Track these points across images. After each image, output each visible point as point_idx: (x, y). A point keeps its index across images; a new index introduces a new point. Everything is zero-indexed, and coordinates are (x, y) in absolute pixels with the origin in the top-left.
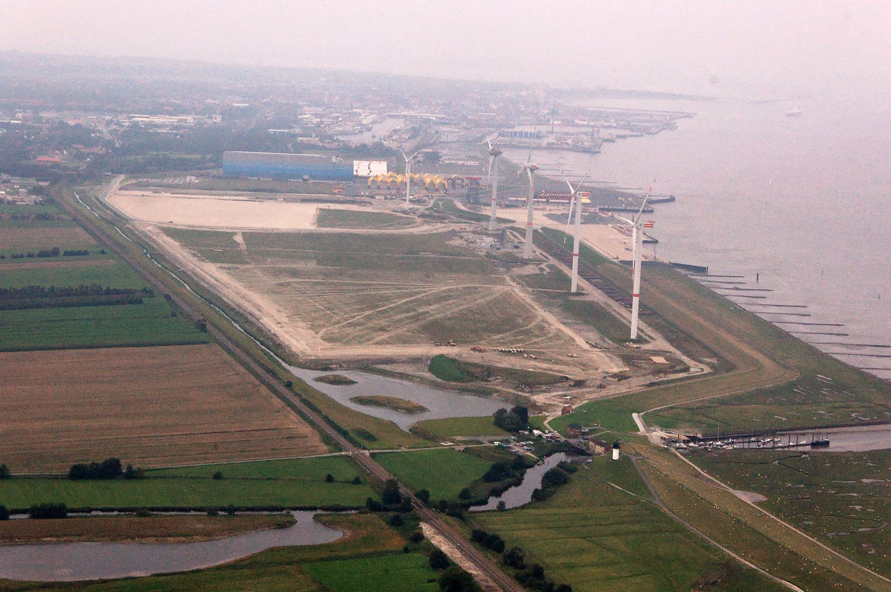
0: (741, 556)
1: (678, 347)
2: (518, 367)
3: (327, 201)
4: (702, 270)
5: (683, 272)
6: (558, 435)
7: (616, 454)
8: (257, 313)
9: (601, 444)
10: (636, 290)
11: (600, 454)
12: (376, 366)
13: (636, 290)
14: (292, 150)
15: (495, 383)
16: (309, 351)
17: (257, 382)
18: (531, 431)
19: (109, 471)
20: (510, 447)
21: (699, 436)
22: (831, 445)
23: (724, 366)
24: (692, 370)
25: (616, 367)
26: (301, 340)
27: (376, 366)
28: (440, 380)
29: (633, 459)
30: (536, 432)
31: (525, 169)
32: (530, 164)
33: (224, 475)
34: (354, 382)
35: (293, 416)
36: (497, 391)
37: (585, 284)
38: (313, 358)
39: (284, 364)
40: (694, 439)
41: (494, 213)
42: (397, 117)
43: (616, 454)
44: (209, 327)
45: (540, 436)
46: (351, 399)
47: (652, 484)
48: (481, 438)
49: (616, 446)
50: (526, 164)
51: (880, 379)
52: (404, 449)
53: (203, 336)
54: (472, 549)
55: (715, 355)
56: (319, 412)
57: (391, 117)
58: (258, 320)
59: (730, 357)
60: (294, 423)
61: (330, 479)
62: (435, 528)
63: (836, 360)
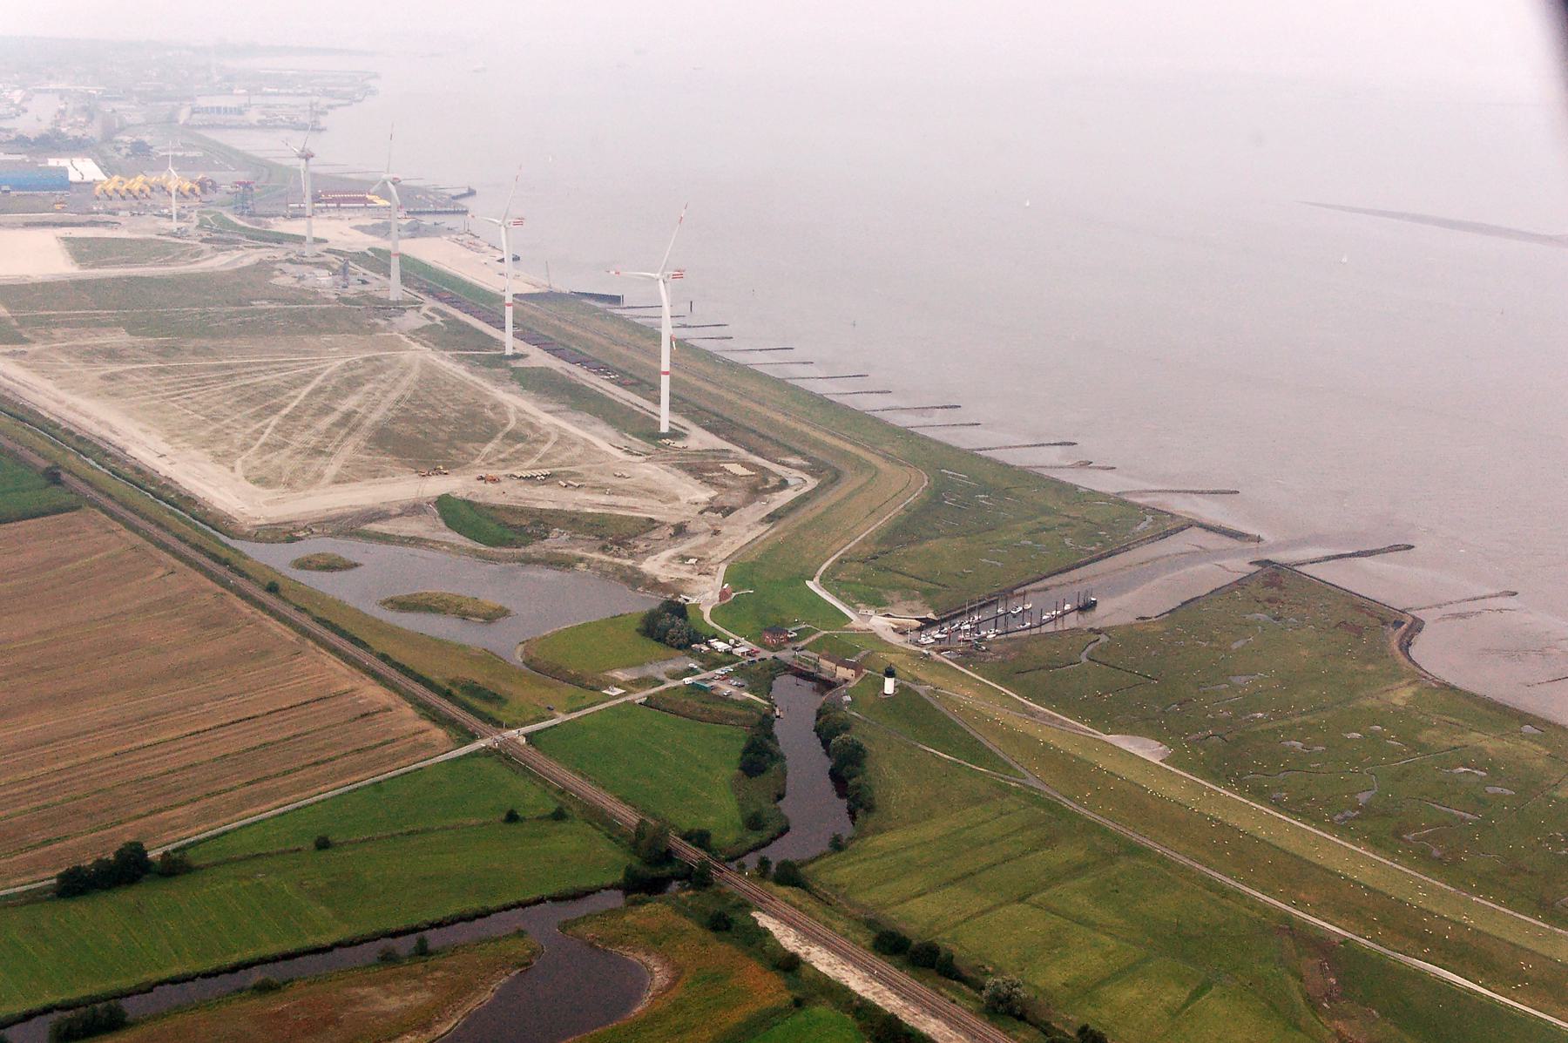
0: (1294, 906)
1: (730, 440)
2: (570, 507)
3: (72, 225)
4: (616, 300)
5: (599, 305)
6: (755, 648)
7: (889, 686)
8: (106, 433)
9: (848, 666)
10: (665, 365)
11: (846, 681)
12: (367, 527)
13: (665, 365)
14: (395, 261)
15: (558, 542)
16: (247, 509)
17: (219, 589)
18: (708, 644)
19: (129, 869)
20: (713, 688)
21: (931, 615)
22: (1100, 610)
23: (827, 472)
24: (791, 482)
25: (704, 495)
26: (225, 489)
27: (367, 527)
28: (482, 548)
29: (921, 690)
30: (721, 646)
31: (385, 183)
32: (391, 176)
33: (334, 838)
34: (356, 565)
35: (332, 661)
36: (581, 560)
37: (523, 347)
38: (263, 522)
39: (223, 538)
40: (928, 624)
41: (310, 229)
42: (47, 91)
43: (889, 686)
44: (65, 476)
45: (728, 653)
46: (384, 603)
47: (992, 743)
48: (651, 670)
50: (385, 176)
51: (965, 452)
52: (561, 718)
53: (57, 495)
54: (881, 964)
55: (794, 452)
56: (364, 645)
57: (40, 91)
58: (123, 451)
59: (815, 453)
60: (336, 673)
61: (512, 817)
62: (795, 927)
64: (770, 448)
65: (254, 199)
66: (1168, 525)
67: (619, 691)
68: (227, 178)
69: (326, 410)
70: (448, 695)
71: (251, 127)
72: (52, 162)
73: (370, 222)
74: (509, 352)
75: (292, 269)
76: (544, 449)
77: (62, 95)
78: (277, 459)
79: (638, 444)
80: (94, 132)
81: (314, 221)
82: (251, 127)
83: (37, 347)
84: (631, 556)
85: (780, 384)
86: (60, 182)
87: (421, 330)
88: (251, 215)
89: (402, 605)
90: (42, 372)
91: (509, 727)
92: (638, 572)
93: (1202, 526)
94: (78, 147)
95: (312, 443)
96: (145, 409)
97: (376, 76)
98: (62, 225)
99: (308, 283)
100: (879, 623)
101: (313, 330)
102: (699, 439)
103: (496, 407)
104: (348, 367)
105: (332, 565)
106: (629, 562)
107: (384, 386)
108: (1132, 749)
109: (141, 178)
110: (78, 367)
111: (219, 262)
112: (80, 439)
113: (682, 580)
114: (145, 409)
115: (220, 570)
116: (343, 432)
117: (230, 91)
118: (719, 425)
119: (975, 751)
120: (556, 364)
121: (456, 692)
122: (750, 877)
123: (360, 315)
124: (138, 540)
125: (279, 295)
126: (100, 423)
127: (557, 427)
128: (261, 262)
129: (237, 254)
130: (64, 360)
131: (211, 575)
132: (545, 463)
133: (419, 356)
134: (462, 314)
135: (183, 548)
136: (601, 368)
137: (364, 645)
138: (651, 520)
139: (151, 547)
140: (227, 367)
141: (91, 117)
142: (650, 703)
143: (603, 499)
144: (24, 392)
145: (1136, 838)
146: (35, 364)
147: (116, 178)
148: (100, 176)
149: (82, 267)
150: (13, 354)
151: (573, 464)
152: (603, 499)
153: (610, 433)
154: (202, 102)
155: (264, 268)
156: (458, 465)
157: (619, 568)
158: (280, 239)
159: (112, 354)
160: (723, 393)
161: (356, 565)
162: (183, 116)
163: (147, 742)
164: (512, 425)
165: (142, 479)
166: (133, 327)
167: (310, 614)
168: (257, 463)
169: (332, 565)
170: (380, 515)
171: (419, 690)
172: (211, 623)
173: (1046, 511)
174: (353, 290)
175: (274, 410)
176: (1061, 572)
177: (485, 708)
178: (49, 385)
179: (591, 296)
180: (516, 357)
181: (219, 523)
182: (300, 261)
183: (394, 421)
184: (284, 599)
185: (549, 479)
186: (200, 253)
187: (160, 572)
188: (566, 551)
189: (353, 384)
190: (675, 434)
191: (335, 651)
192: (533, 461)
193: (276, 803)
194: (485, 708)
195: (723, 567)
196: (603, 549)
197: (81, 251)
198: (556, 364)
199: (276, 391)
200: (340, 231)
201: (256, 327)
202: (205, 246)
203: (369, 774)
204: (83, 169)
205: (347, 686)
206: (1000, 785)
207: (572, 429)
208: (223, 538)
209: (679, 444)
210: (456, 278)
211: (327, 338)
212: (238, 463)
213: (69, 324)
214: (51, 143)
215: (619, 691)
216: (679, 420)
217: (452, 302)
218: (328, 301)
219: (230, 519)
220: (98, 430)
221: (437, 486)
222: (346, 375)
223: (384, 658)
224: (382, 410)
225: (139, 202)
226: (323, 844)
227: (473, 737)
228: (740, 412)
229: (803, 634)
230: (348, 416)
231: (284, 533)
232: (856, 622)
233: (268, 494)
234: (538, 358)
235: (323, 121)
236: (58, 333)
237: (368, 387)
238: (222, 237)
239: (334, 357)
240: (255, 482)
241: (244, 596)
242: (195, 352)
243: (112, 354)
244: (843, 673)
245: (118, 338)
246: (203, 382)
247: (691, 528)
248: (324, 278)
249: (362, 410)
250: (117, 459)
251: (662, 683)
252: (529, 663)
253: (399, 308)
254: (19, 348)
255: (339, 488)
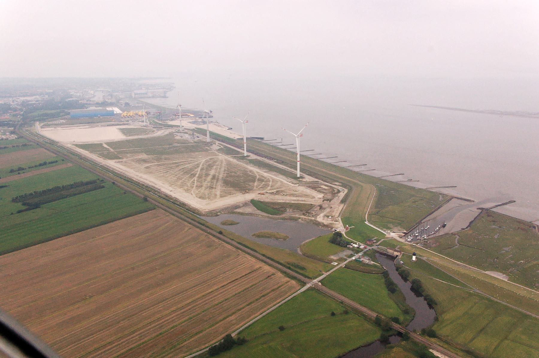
1: (316, 178)
4: (262, 139)
5: (259, 140)
7: (414, 258)
8: (154, 185)
10: (298, 160)
11: (397, 256)
13: (298, 160)
15: (289, 213)
16: (201, 207)
24: (340, 190)
29: (424, 258)
30: (356, 246)
33: (285, 325)
34: (238, 223)
35: (249, 257)
37: (250, 154)
39: (198, 216)
41: (208, 127)
43: (414, 258)
44: (148, 199)
45: (358, 248)
47: (456, 278)
49: (414, 255)
55: (337, 181)
56: (255, 251)
61: (333, 314)
63: (384, 180)
64: (329, 180)
65: (161, 117)
66: (449, 199)
67: (336, 263)
68: (153, 111)
69: (207, 175)
70: (289, 268)
71: (150, 97)
72: (108, 109)
73: (192, 121)
74: (245, 155)
75: (179, 134)
76: (270, 183)
77: (103, 91)
78: (202, 190)
79: (295, 181)
80: (114, 100)
81: (209, 125)
82: (150, 97)
83: (124, 160)
84: (313, 216)
85: (317, 160)
86: (112, 114)
87: (219, 150)
88: (161, 120)
89: (258, 236)
90: (128, 167)
91: (314, 279)
92: (316, 221)
93: (456, 198)
94: (112, 104)
95: (209, 185)
96: (160, 177)
97: (174, 84)
98: (118, 125)
99: (184, 138)
100: (393, 235)
101: (191, 151)
102: (308, 178)
103: (251, 171)
104: (207, 161)
105: (232, 224)
106: (313, 218)
107: (219, 167)
108: (492, 275)
109: (131, 112)
110: (137, 165)
111: (160, 133)
112: (147, 187)
113: (330, 223)
114: (160, 177)
115: (203, 227)
116: (215, 181)
117: (141, 89)
118: (311, 174)
119: (456, 282)
120: (259, 158)
121: (291, 267)
122: (420, 334)
123: (199, 147)
124: (176, 218)
125: (178, 142)
126: (150, 182)
127: (272, 178)
128: (170, 133)
129: (163, 131)
130: (133, 163)
131: (202, 230)
132: (273, 188)
133: (222, 157)
134: (230, 146)
135: (190, 220)
136: (271, 159)
137: (255, 251)
138: (311, 204)
139: (180, 220)
140: (176, 163)
141: (112, 97)
142: (347, 267)
143: (295, 198)
144: (127, 173)
145: (524, 311)
146: (125, 164)
147: (126, 112)
148: (121, 112)
149: (127, 136)
150: (119, 162)
151: (280, 188)
152: (295, 198)
153: (284, 177)
154: (136, 92)
155: (171, 134)
156: (251, 190)
157: (311, 220)
158: (172, 126)
159: (145, 161)
160: (305, 164)
161: (238, 223)
162: (133, 96)
163: (210, 291)
164: (258, 177)
165: (168, 198)
166: (147, 152)
167: (235, 241)
168: (197, 192)
169: (232, 224)
170: (237, 207)
171: (280, 266)
172: (210, 245)
173: (413, 196)
174: (196, 139)
175: (194, 175)
176: (430, 214)
177: (301, 272)
178: (132, 171)
179: (257, 138)
180: (248, 156)
181: (194, 211)
182: (179, 132)
183: (227, 177)
184: (224, 235)
185: (278, 193)
186: (153, 131)
187: (186, 229)
188: (294, 216)
189: (210, 167)
190: (302, 177)
191: (249, 254)
192: (269, 188)
193: (259, 313)
194: (301, 272)
195: (340, 219)
196: (304, 214)
197: (124, 132)
198: (259, 158)
199: (191, 170)
200: (185, 123)
201: (177, 151)
202: (154, 129)
203: (281, 299)
204: (117, 110)
205: (258, 266)
206: (467, 292)
207: (265, 174)
208: (198, 216)
209: (304, 180)
210: (227, 137)
211: (197, 153)
212: (192, 192)
213: (130, 153)
214: (104, 104)
215: (336, 263)
216: (302, 174)
217: (223, 141)
218: (191, 143)
219: (198, 210)
220: (150, 184)
221: (249, 197)
222: (207, 164)
223: (264, 255)
224: (222, 173)
225: (133, 118)
226: (282, 329)
227: (304, 284)
228: (320, 172)
229: (378, 240)
230: (214, 177)
231: (214, 213)
232: (387, 236)
233: (205, 202)
234: (253, 157)
235: (167, 95)
236: (128, 155)
237: (215, 167)
238: (159, 127)
239: (202, 159)
240: (200, 198)
241: (214, 236)
242: (166, 159)
243: (145, 161)
244: (396, 253)
245: (144, 156)
246: (171, 168)
247: (324, 206)
248: (187, 137)
249: (217, 174)
250: (159, 193)
251: (346, 260)
252: (304, 255)
253: (211, 144)
254: (120, 160)
255: (222, 199)
